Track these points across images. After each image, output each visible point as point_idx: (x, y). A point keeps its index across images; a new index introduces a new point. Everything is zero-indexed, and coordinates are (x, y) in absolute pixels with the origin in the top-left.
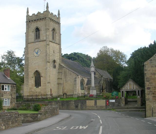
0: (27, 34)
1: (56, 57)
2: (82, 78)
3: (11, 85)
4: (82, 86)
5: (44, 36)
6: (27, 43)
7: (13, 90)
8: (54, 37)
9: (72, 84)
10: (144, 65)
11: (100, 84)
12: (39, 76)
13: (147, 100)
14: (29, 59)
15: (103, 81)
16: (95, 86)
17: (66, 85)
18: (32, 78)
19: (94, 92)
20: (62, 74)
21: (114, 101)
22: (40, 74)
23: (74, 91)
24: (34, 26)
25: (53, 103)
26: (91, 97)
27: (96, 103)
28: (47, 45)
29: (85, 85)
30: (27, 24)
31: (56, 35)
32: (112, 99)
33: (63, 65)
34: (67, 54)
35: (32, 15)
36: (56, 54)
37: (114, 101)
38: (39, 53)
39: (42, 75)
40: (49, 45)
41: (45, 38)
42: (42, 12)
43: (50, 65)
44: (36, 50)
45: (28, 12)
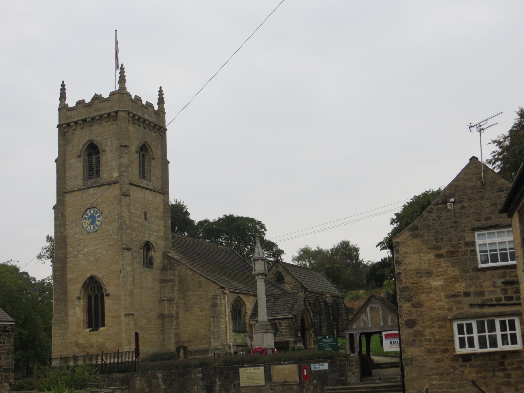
0: (61, 163)
1: (155, 234)
2: (236, 295)
3: (501, 303)
4: (237, 321)
5: (112, 170)
6: (63, 191)
7: (4, 343)
8: (146, 172)
9: (206, 315)
10: (394, 245)
11: (293, 313)
12: (99, 294)
13: (407, 365)
14: (68, 240)
15: (305, 302)
16: (268, 320)
17: (187, 320)
18: (77, 302)
19: (265, 340)
20: (173, 287)
21: (325, 366)
22: (103, 287)
23: (210, 338)
24: (81, 138)
25: (138, 378)
26: (255, 357)
27: (268, 376)
28: (123, 197)
29: (248, 317)
30: (60, 132)
31: (152, 164)
32: (320, 360)
33: (176, 257)
34: (206, 221)
35: (77, 104)
36: (152, 223)
37: (325, 366)
38: (99, 221)
39: (108, 292)
40: (128, 198)
41: (116, 175)
42: (106, 95)
43: (134, 258)
44: (88, 212)
45: (63, 96)
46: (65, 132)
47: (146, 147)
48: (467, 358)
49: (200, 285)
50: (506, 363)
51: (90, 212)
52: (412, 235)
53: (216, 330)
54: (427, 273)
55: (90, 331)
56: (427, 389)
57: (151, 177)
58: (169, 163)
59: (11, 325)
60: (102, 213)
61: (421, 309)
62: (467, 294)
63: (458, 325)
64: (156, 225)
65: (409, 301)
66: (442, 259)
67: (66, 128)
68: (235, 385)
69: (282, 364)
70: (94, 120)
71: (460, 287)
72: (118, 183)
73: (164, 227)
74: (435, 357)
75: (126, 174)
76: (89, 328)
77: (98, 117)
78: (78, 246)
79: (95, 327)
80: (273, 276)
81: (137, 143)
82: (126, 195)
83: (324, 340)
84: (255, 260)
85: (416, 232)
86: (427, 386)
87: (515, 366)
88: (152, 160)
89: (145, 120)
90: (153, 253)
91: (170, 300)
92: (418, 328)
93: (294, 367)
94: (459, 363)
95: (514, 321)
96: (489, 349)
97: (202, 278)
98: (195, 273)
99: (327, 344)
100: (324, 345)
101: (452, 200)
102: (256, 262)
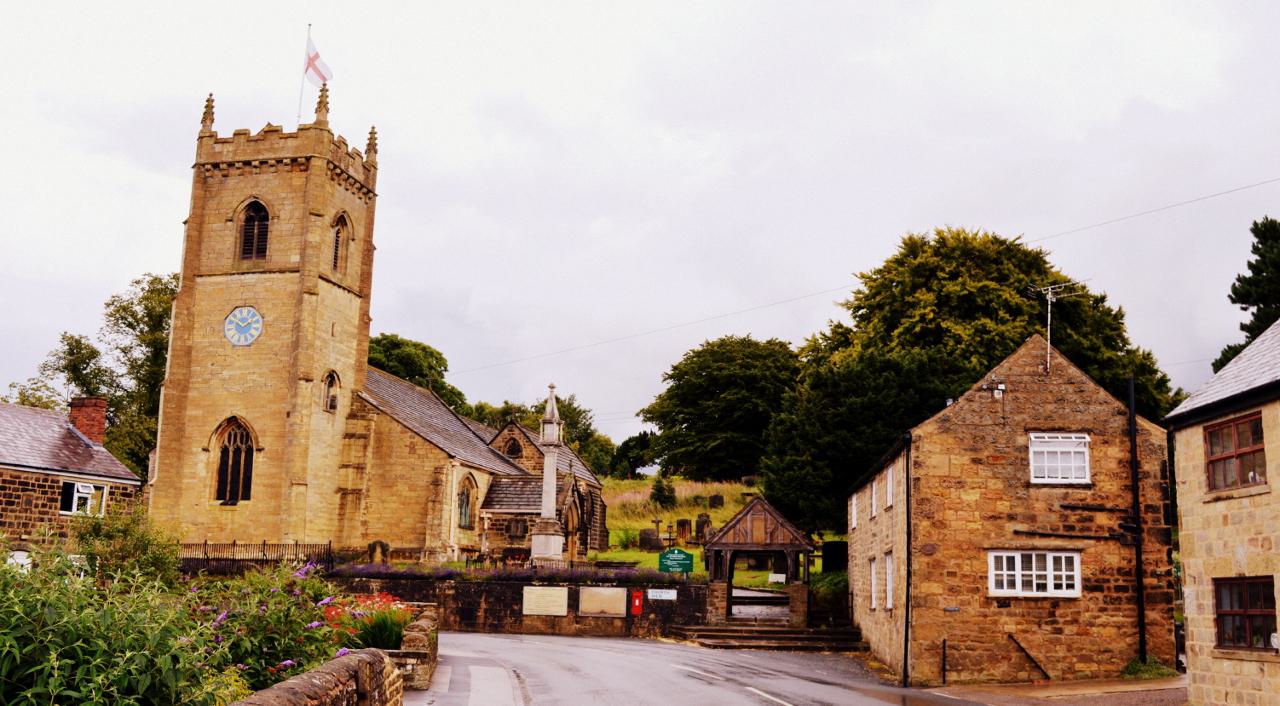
2: (467, 470)
10: (914, 438)
14: (193, 353)
15: (573, 491)
17: (383, 502)
20: (365, 447)
21: (671, 595)
22: (252, 436)
24: (236, 194)
27: (574, 601)
37: (671, 595)
38: (257, 329)
39: (261, 445)
40: (314, 297)
45: (208, 115)
46: (206, 178)
47: (345, 221)
48: (1004, 602)
49: (412, 448)
50: (1057, 613)
51: (241, 312)
52: (940, 428)
53: (436, 522)
54: (958, 483)
55: (221, 504)
56: (944, 641)
57: (346, 268)
58: (375, 249)
59: (135, 486)
60: (263, 318)
61: (946, 531)
62: (1011, 518)
63: (996, 558)
64: (347, 347)
65: (929, 518)
66: (980, 466)
67: (210, 171)
68: (513, 611)
69: (599, 586)
70: (264, 166)
71: (1003, 507)
72: (298, 271)
73: (357, 350)
74: (959, 597)
75: (315, 260)
76: (218, 498)
77: (288, 161)
78: (212, 365)
79: (230, 499)
80: (503, 444)
81: (334, 212)
82: (312, 294)
83: (671, 556)
84: (545, 422)
85: (947, 425)
86: (945, 636)
87: (1069, 619)
88: (351, 242)
89: (349, 177)
90: (338, 389)
91: (360, 468)
92: (938, 556)
93: (620, 593)
94: (992, 609)
95: (1013, 558)
96: (1034, 593)
97: (417, 438)
98: (405, 429)
99: (675, 562)
100: (669, 563)
101: (1002, 387)
102: (547, 426)
